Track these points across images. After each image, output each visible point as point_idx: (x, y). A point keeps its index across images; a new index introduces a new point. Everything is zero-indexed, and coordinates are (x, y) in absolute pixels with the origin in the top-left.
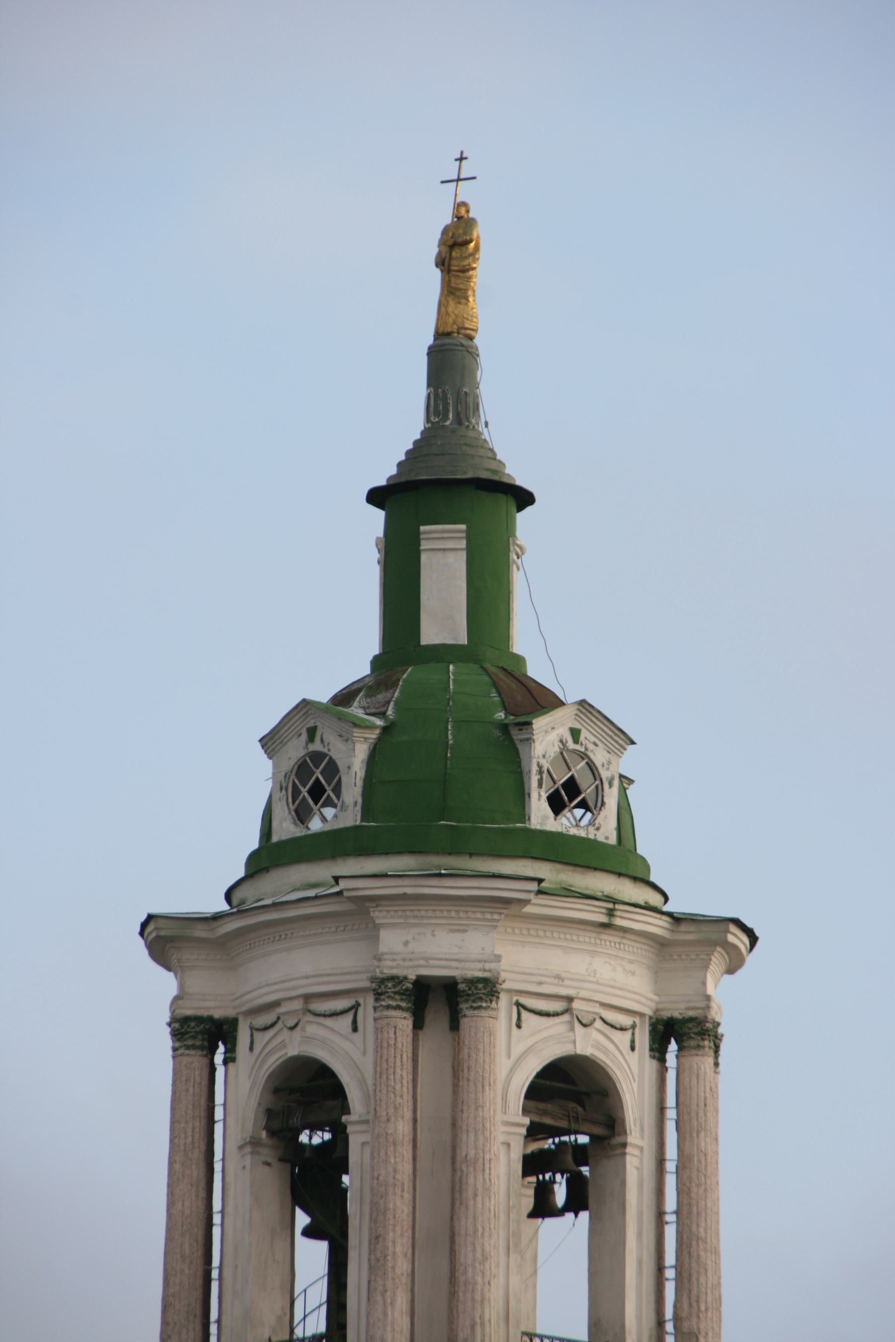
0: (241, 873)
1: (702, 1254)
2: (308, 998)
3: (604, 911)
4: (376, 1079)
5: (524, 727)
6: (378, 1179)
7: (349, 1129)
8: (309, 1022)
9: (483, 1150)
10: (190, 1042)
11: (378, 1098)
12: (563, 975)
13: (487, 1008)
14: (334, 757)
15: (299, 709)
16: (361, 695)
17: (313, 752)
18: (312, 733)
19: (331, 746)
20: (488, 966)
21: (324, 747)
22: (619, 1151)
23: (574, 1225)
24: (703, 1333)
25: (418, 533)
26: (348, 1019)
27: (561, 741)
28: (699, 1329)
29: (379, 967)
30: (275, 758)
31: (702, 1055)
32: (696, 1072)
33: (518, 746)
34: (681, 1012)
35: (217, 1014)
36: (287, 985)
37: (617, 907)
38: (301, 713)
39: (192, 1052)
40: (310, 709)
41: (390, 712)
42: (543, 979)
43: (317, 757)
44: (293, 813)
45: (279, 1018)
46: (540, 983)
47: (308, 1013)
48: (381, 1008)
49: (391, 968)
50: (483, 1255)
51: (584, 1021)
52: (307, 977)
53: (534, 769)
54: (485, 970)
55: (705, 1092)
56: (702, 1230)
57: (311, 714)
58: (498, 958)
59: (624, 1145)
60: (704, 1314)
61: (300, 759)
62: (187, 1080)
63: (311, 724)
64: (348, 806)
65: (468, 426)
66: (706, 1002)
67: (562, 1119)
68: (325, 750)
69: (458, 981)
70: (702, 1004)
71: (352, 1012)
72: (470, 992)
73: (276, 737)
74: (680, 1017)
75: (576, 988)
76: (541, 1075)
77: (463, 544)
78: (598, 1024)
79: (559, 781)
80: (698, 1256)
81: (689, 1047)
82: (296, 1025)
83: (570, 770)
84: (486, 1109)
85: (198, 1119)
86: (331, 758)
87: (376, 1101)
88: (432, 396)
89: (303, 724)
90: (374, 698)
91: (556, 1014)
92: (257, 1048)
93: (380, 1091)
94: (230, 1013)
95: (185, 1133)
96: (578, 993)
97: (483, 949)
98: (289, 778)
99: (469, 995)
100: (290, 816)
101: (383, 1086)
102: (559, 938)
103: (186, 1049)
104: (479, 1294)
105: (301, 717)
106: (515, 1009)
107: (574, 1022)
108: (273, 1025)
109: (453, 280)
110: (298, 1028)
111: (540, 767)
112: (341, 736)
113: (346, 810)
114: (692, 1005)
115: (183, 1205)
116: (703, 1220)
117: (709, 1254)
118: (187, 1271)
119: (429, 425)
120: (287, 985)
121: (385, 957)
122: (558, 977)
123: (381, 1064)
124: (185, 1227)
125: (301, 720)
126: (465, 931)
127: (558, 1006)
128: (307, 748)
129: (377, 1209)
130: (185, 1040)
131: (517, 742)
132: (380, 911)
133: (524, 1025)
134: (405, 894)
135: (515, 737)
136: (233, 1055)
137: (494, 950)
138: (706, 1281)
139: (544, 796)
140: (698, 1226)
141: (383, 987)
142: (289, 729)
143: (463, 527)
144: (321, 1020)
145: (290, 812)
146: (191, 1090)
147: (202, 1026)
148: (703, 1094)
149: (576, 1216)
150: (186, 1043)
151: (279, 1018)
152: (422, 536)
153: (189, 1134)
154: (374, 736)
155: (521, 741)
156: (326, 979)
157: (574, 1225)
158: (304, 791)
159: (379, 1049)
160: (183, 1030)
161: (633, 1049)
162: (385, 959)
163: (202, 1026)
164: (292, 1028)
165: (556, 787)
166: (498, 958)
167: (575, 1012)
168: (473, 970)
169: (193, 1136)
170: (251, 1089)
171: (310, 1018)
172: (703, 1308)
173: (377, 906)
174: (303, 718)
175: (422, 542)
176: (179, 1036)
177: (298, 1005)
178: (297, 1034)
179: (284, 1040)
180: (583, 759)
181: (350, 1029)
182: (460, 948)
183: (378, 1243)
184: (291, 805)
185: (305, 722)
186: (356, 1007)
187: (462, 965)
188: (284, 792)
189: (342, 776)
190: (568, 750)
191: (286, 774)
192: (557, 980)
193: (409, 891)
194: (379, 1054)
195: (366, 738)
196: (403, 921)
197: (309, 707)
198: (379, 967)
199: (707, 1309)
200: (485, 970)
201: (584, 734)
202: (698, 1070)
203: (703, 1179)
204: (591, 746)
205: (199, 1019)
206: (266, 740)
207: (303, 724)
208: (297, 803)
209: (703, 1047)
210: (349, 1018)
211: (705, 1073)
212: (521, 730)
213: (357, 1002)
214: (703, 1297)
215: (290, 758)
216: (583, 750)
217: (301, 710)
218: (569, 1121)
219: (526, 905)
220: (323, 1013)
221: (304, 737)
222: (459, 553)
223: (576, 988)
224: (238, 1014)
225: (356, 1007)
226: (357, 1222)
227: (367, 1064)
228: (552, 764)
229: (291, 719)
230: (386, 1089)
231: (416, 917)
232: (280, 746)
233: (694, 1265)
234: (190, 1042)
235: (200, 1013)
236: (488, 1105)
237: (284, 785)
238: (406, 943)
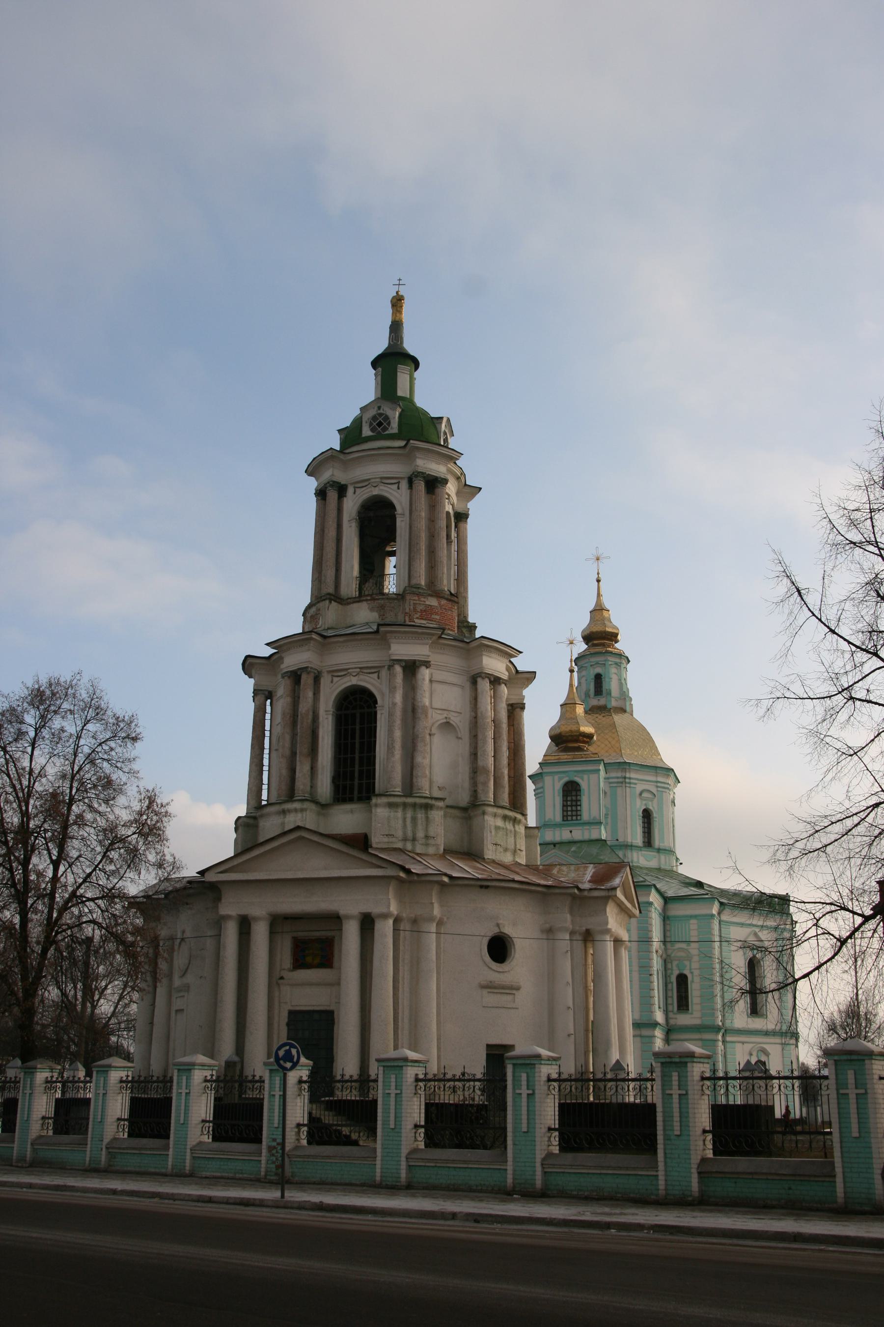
2: (381, 478)
43: (380, 415)
92: (357, 493)
178: (377, 488)
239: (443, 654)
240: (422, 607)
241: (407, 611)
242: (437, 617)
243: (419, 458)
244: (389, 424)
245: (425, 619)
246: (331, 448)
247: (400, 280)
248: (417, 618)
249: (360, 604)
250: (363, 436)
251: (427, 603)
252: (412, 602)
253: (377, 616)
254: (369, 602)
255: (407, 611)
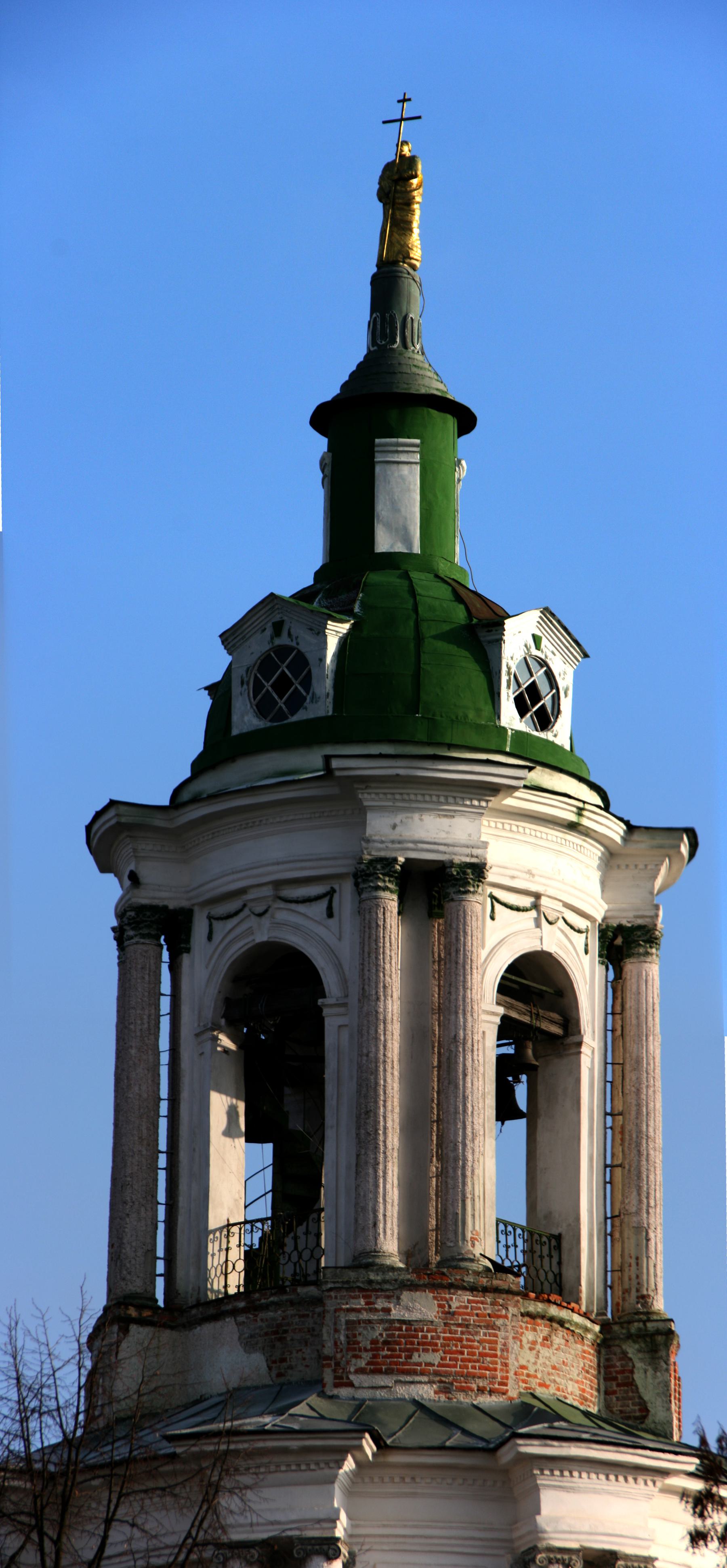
0: (187, 774)
1: (652, 1152)
2: (278, 884)
3: (575, 809)
4: (363, 959)
5: (494, 629)
6: (367, 1055)
7: (326, 1012)
8: (279, 909)
9: (472, 1031)
10: (145, 931)
11: (366, 977)
12: (534, 872)
13: (474, 893)
14: (303, 650)
15: (265, 603)
16: (320, 596)
17: (279, 646)
18: (278, 628)
19: (299, 640)
20: (475, 852)
21: (292, 641)
22: (573, 1051)
23: (501, 1131)
24: (652, 1228)
25: (373, 445)
26: (323, 905)
27: (526, 646)
28: (648, 1224)
29: (367, 849)
30: (235, 654)
31: (650, 962)
32: (644, 978)
33: (486, 648)
34: (629, 920)
35: (172, 905)
36: (255, 872)
37: (587, 806)
38: (269, 606)
39: (147, 941)
40: (277, 604)
41: (357, 609)
42: (516, 873)
43: (283, 652)
44: (255, 707)
45: (245, 906)
46: (513, 877)
47: (279, 901)
48: (370, 889)
49: (380, 850)
50: (473, 1133)
51: (550, 919)
52: (278, 863)
53: (504, 669)
54: (472, 856)
55: (653, 998)
56: (651, 1130)
57: (278, 609)
58: (485, 845)
59: (580, 1044)
60: (654, 1210)
61: (264, 654)
62: (142, 968)
63: (277, 618)
64: (319, 698)
65: (413, 351)
66: (655, 911)
67: (525, 1014)
68: (294, 644)
69: (446, 865)
70: (652, 913)
71: (327, 898)
72: (458, 877)
73: (239, 632)
74: (629, 925)
75: (544, 885)
76: (513, 968)
77: (417, 458)
78: (561, 923)
79: (524, 684)
80: (648, 1155)
81: (638, 954)
82: (266, 911)
83: (532, 675)
84: (474, 991)
85: (153, 1007)
86: (299, 651)
87: (364, 980)
88: (378, 320)
89: (268, 619)
90: (335, 599)
91: (525, 910)
92: (217, 937)
93: (369, 970)
94: (185, 904)
95: (142, 1019)
96: (546, 891)
97: (470, 835)
98: (251, 673)
99: (457, 879)
100: (252, 711)
101: (371, 965)
102: (531, 835)
103: (141, 938)
104: (469, 1170)
105: (266, 612)
106: (489, 900)
107: (541, 919)
108: (236, 913)
109: (398, 213)
110: (268, 915)
111: (509, 668)
112: (311, 629)
113: (316, 702)
114: (640, 913)
115: (140, 1089)
116: (652, 1119)
117: (657, 1153)
118: (144, 1152)
119: (375, 348)
120: (255, 872)
121: (374, 838)
122: (529, 872)
123: (369, 945)
124: (142, 1111)
125: (267, 614)
126: (453, 817)
127: (526, 901)
128: (273, 643)
129: (367, 1085)
130: (140, 929)
131: (484, 644)
132: (369, 793)
133: (497, 916)
134: (398, 775)
135: (482, 639)
136: (188, 946)
137: (480, 837)
138: (655, 1179)
139: (512, 697)
140: (647, 1126)
141: (371, 868)
142: (252, 624)
143: (418, 441)
144: (293, 906)
145: (251, 707)
146: (147, 977)
147: (157, 917)
148: (651, 1000)
149: (503, 1124)
150: (141, 931)
151: (245, 906)
152: (376, 449)
153: (146, 1020)
154: (345, 631)
155: (489, 642)
156: (299, 865)
157: (501, 1131)
158: (268, 686)
159: (367, 930)
160: (138, 919)
161: (586, 952)
162: (374, 841)
163: (157, 917)
164: (260, 915)
165: (521, 690)
166: (485, 845)
167: (543, 909)
168: (461, 855)
169: (149, 1023)
170: (209, 980)
171: (282, 905)
172: (652, 1203)
173: (367, 788)
174: (269, 612)
175: (376, 454)
176: (133, 926)
177: (268, 891)
178: (266, 921)
179: (251, 927)
180: (542, 666)
181: (325, 915)
182: (448, 833)
183: (368, 1118)
184: (252, 700)
185: (270, 617)
186: (331, 893)
187: (451, 849)
188: (245, 686)
189: (312, 668)
190: (531, 656)
191: (248, 669)
192: (528, 876)
193: (402, 772)
194: (367, 935)
195: (337, 632)
196: (391, 804)
197: (276, 601)
198: (367, 849)
199: (656, 1206)
200: (472, 856)
201: (544, 642)
202: (646, 977)
203: (652, 1082)
204: (550, 655)
205: (153, 909)
206: (227, 634)
207: (268, 619)
208: (259, 697)
209: (652, 954)
210: (324, 904)
211: (653, 979)
212: (489, 631)
213: (332, 888)
214: (652, 1192)
215: (252, 653)
216: (543, 657)
217: (267, 605)
218: (531, 1017)
219: (517, 791)
220: (295, 899)
221: (269, 632)
222: (414, 466)
223: (544, 885)
224: (193, 905)
225: (331, 893)
226: (334, 1102)
227: (347, 949)
228: (517, 667)
229: (257, 613)
230: (374, 968)
231: (403, 800)
232: (242, 641)
233: (644, 1163)
234: (145, 931)
235: (155, 902)
236: (475, 987)
237: (246, 679)
238: (394, 827)
239: (414, 1495)
240: (378, 1333)
241: (328, 1350)
242: (435, 1358)
243: (373, 808)
244: (307, 683)
245: (389, 1372)
246: (112, 803)
247: (404, 100)
248: (360, 1371)
249: (219, 1324)
250: (235, 732)
251: (396, 1313)
252: (343, 1319)
253: (264, 1366)
254: (241, 1318)
255: (328, 1350)
